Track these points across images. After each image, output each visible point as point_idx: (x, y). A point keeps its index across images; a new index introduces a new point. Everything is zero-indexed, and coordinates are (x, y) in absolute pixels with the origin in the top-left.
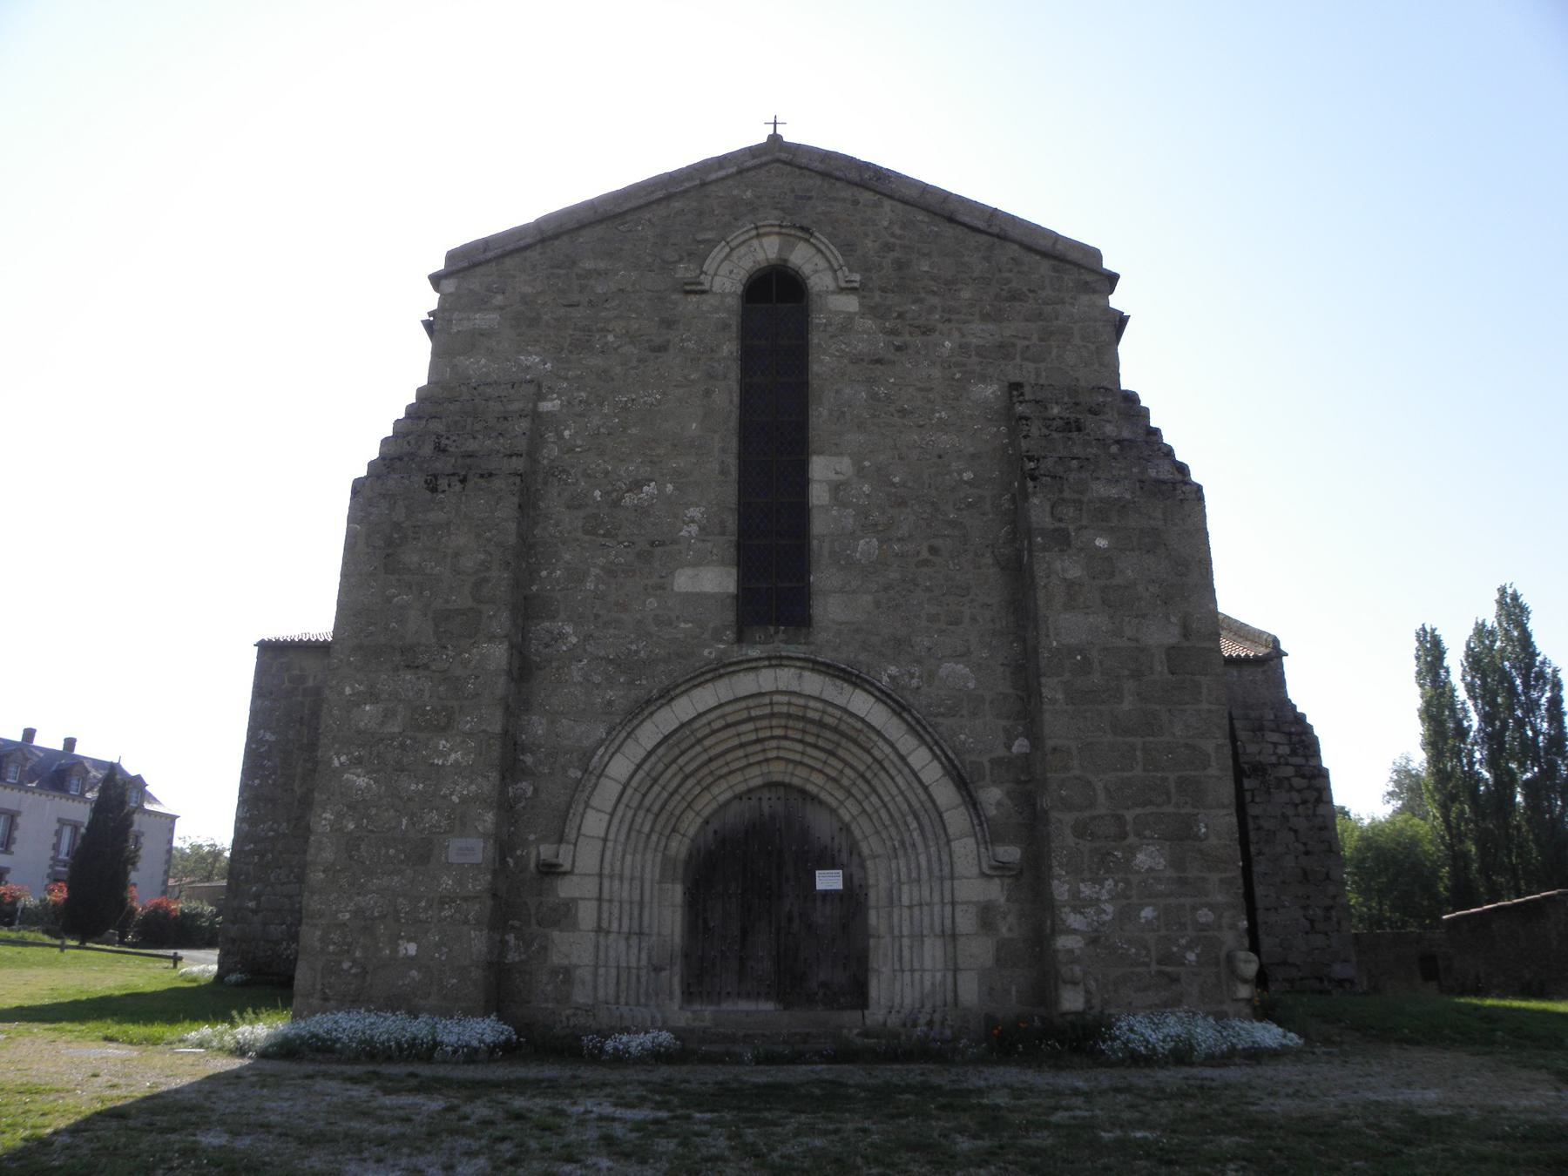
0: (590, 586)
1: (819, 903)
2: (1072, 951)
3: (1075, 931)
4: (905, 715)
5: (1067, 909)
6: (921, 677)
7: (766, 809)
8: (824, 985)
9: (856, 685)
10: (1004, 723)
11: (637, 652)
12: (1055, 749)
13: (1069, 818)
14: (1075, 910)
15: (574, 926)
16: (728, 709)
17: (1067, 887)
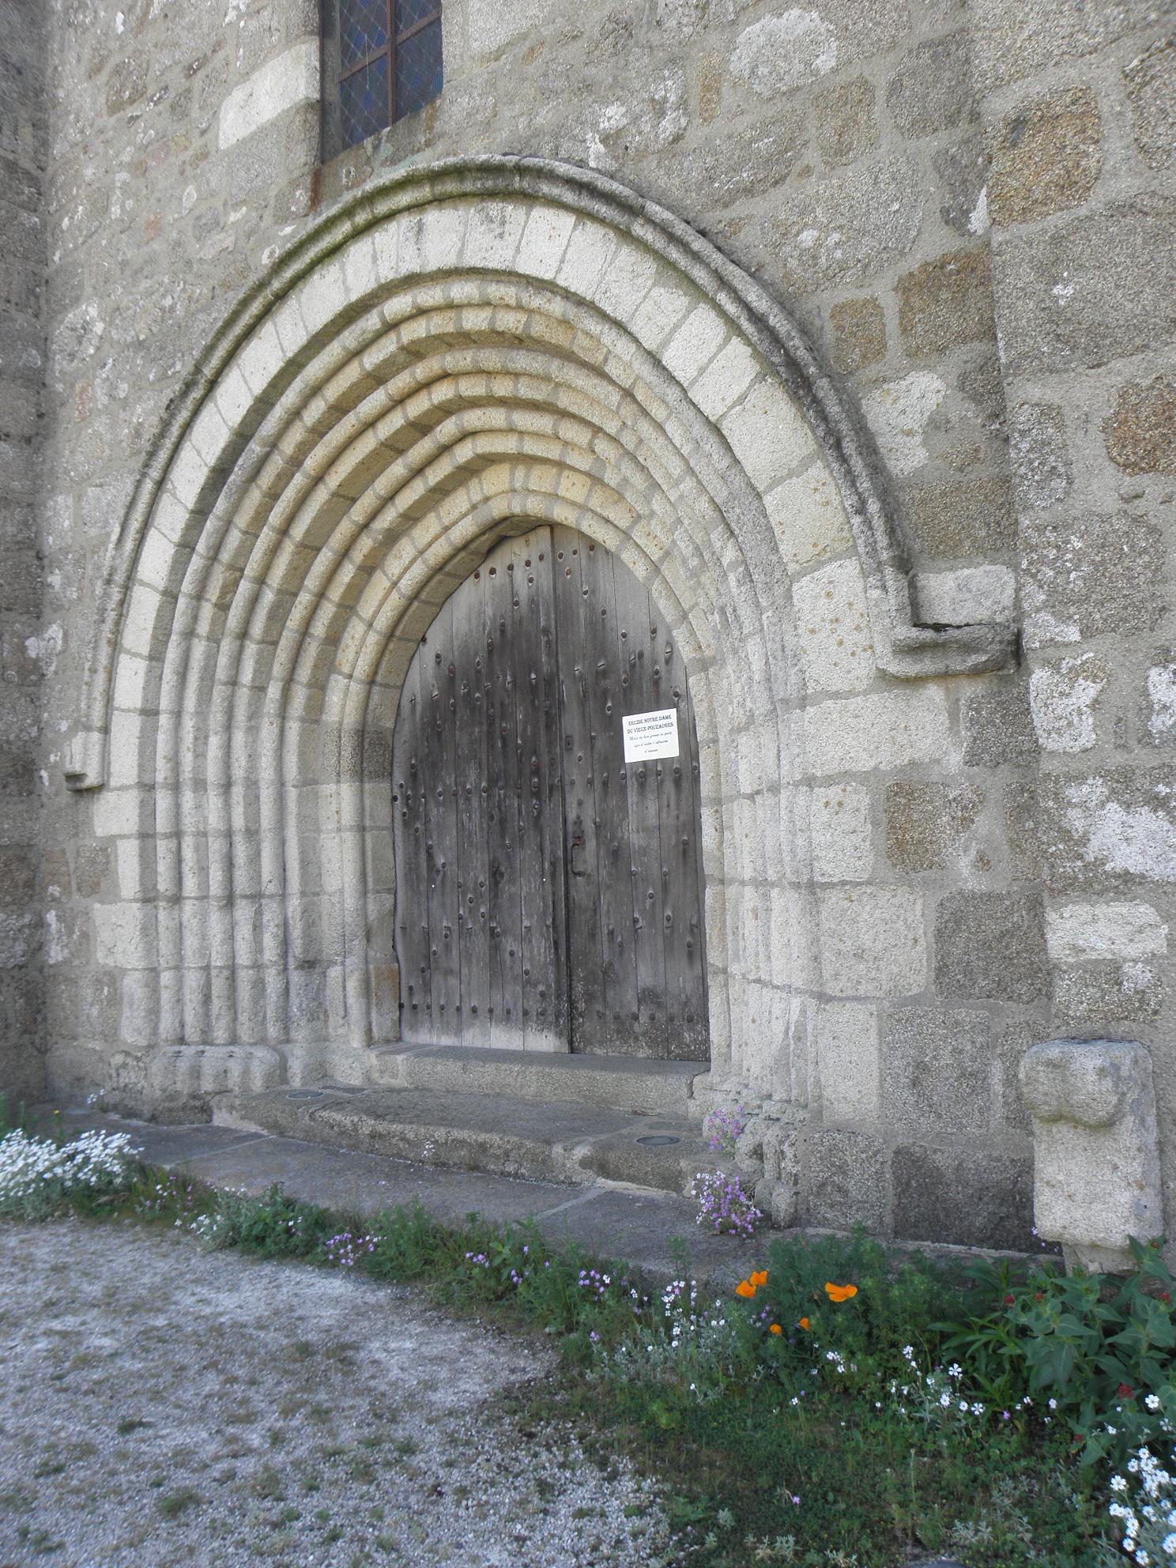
0: (115, 211)
1: (632, 797)
2: (1111, 971)
3: (1127, 884)
4: (639, 229)
5: (1094, 789)
6: (683, 103)
7: (523, 591)
8: (649, 996)
9: (529, 198)
10: (933, 143)
11: (172, 309)
12: (1018, 124)
13: (1090, 393)
14: (1126, 788)
15: (113, 896)
16: (315, 369)
17: (1087, 691)
